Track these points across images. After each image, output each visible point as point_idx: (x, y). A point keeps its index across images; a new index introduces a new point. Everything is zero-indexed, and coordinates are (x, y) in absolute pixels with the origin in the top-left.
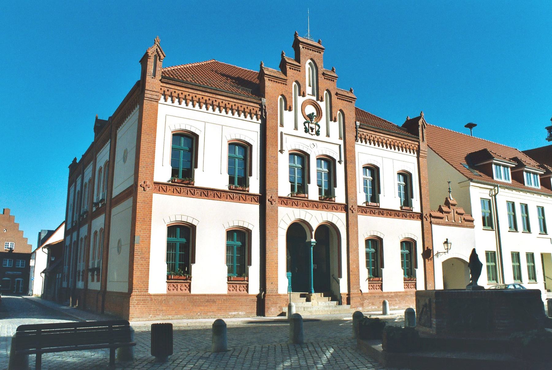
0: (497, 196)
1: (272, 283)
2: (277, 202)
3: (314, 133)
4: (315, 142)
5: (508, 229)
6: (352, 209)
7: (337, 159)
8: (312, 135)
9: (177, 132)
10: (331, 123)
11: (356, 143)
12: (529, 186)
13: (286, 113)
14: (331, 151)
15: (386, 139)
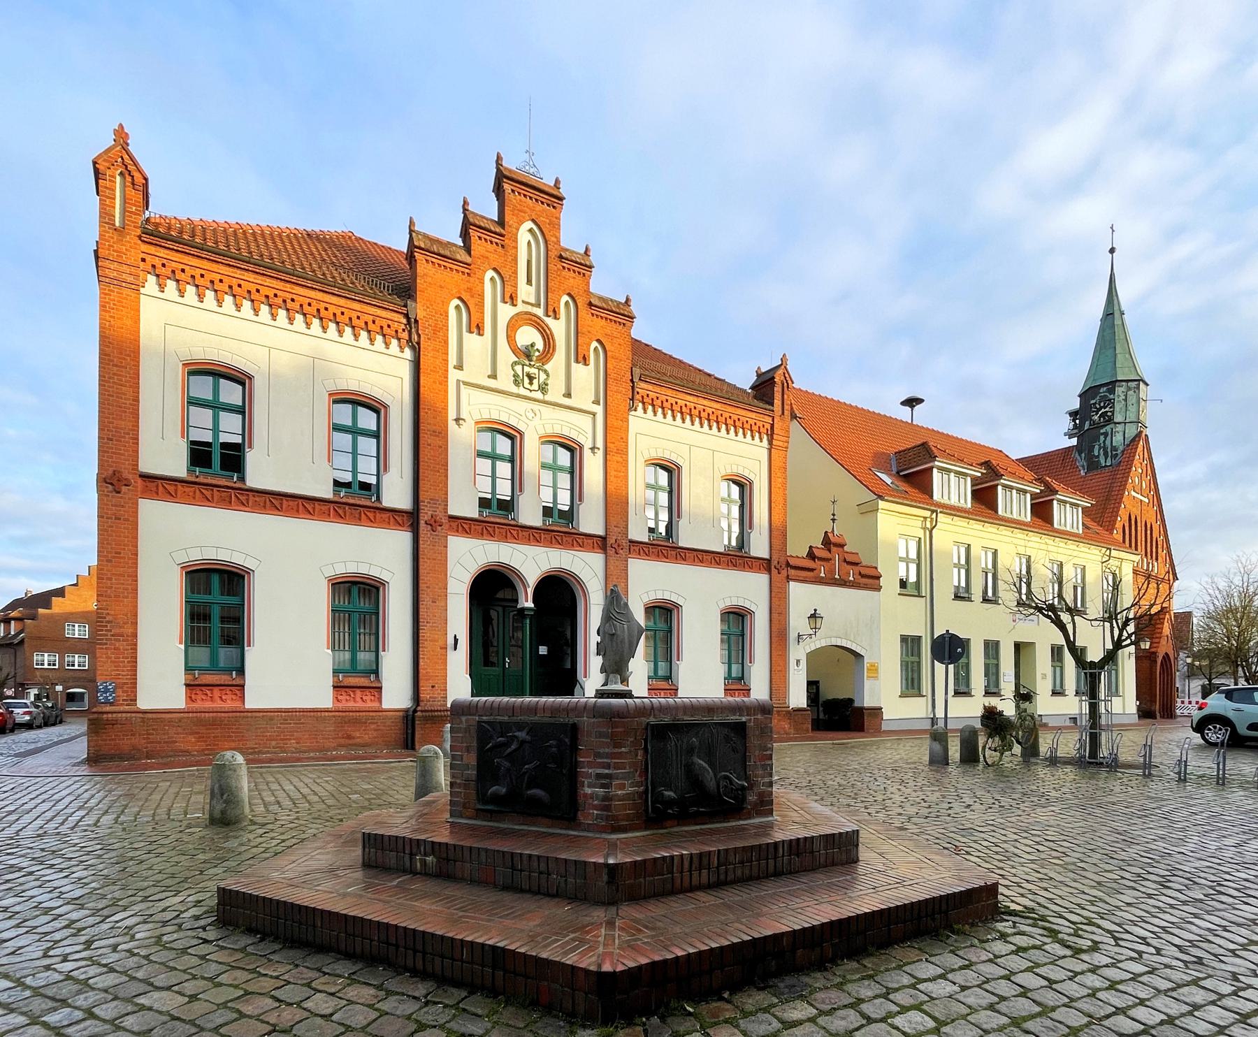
0: (934, 531)
1: (433, 687)
2: (446, 526)
3: (535, 386)
4: (536, 406)
5: (898, 590)
6: (616, 546)
7: (587, 445)
8: (531, 391)
9: (232, 372)
10: (577, 368)
11: (633, 413)
12: (1008, 515)
13: (471, 340)
14: (502, 409)
15: (727, 415)
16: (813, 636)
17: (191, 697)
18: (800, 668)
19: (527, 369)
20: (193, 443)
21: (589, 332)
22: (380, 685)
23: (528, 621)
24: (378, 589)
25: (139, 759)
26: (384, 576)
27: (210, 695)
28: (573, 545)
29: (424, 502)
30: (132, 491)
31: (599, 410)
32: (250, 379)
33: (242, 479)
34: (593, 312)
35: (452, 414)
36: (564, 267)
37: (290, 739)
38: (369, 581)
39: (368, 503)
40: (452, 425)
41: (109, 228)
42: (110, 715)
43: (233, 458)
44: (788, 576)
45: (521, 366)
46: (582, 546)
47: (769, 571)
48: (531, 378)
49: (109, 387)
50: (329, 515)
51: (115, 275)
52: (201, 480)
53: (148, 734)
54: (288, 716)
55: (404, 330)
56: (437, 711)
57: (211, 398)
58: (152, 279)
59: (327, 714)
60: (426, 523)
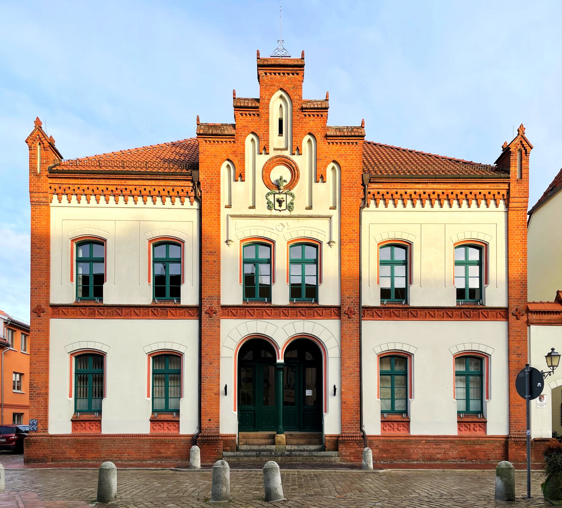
1: (210, 420)
4: (284, 221)
7: (325, 240)
8: (280, 211)
13: (238, 186)
16: (552, 373)
17: (383, 428)
18: (544, 402)
19: (277, 196)
20: (292, 285)
21: (325, 157)
22: (484, 420)
23: (281, 373)
24: (406, 359)
25: (47, 462)
26: (181, 349)
27: (392, 427)
28: (314, 316)
29: (204, 299)
30: (46, 315)
31: (335, 214)
32: (320, 243)
33: (317, 301)
34: (329, 141)
35: (223, 238)
36: (305, 115)
37: (124, 453)
38: (173, 353)
39: (401, 306)
40: (223, 245)
41: (34, 175)
42: (34, 438)
44: (528, 320)
45: (273, 195)
46: (321, 316)
47: (506, 318)
48: (280, 202)
49: (36, 260)
50: (149, 315)
51: (37, 199)
52: (250, 305)
53: (52, 448)
54: (123, 439)
55: (192, 191)
56: (212, 436)
57: (165, 257)
58: (55, 197)
59: (145, 438)
60: (206, 313)
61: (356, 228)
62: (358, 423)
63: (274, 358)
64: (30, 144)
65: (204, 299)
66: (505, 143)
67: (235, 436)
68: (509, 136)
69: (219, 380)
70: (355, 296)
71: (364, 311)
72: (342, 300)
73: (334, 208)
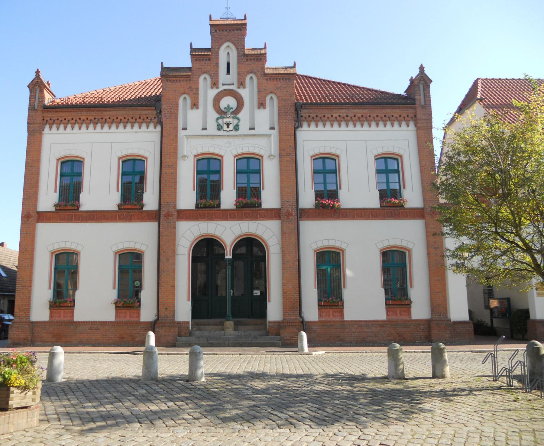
1: (166, 309)
29: (163, 205)
43: (334, 195)
61: (292, 144)
62: (298, 310)
63: (224, 255)
64: (31, 88)
65: (163, 205)
66: (412, 78)
67: (188, 323)
68: (415, 73)
69: (174, 274)
70: (293, 200)
71: (301, 212)
72: (282, 204)
73: (272, 128)
